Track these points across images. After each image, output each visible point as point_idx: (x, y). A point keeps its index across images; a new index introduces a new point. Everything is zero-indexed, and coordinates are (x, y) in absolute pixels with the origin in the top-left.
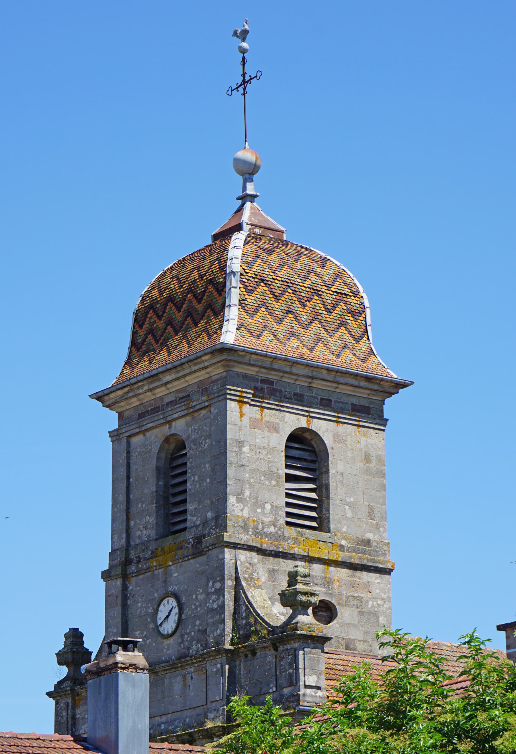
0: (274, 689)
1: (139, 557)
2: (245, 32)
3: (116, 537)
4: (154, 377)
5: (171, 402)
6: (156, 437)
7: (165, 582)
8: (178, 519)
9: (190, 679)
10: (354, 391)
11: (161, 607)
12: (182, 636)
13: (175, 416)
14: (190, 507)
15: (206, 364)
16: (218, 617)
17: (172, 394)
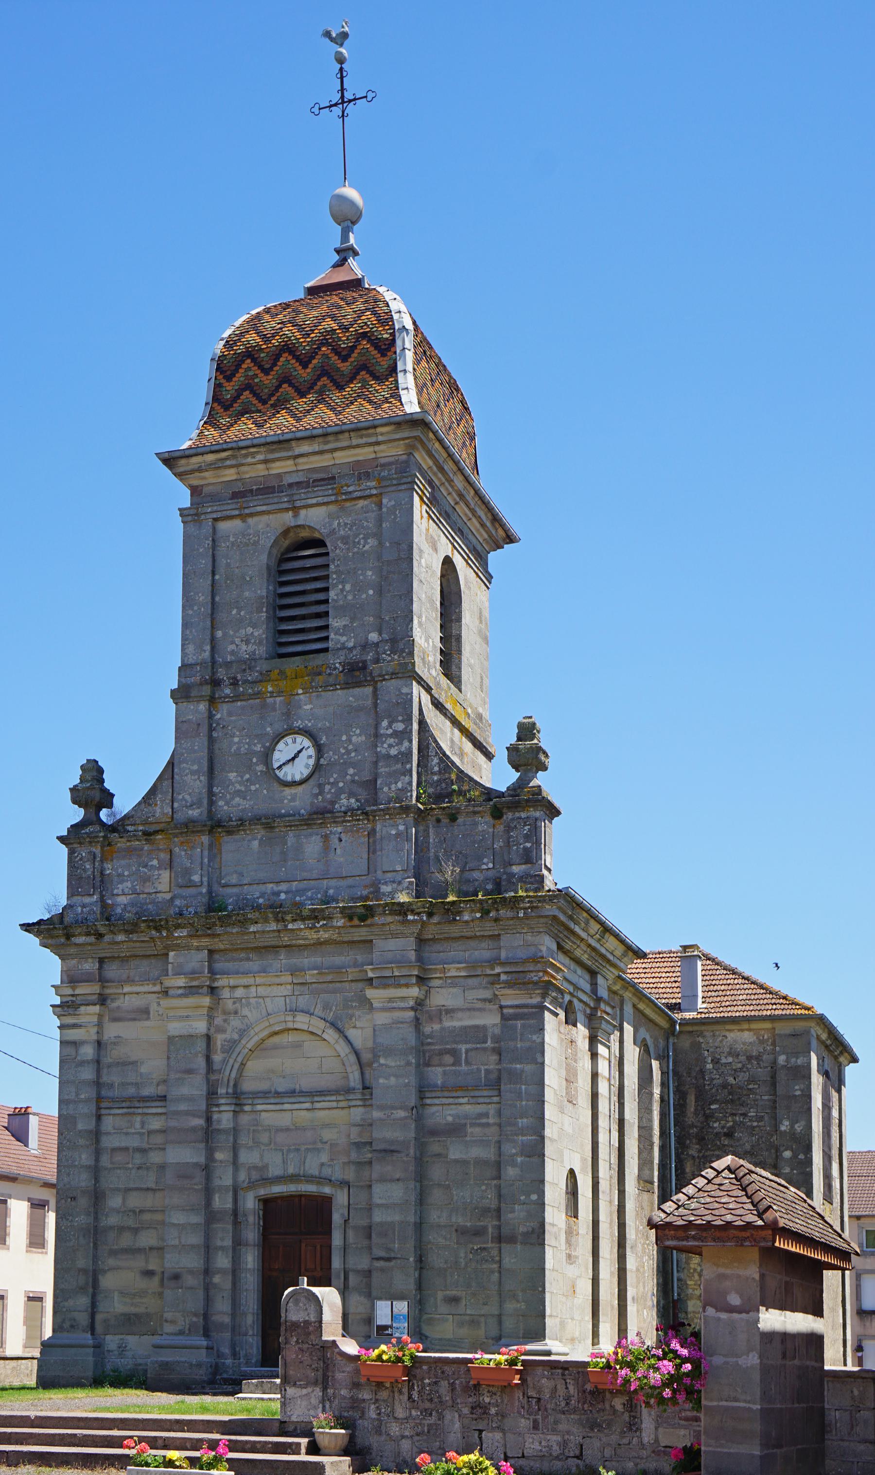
0: (491, 865)
1: (235, 678)
2: (345, 35)
3: (191, 648)
4: (282, 443)
5: (297, 483)
6: (268, 526)
7: (288, 714)
8: (291, 639)
9: (336, 841)
10: (478, 530)
11: (281, 745)
12: (320, 786)
13: (259, 509)
14: (335, 623)
15: (380, 438)
16: (399, 766)
17: (301, 473)
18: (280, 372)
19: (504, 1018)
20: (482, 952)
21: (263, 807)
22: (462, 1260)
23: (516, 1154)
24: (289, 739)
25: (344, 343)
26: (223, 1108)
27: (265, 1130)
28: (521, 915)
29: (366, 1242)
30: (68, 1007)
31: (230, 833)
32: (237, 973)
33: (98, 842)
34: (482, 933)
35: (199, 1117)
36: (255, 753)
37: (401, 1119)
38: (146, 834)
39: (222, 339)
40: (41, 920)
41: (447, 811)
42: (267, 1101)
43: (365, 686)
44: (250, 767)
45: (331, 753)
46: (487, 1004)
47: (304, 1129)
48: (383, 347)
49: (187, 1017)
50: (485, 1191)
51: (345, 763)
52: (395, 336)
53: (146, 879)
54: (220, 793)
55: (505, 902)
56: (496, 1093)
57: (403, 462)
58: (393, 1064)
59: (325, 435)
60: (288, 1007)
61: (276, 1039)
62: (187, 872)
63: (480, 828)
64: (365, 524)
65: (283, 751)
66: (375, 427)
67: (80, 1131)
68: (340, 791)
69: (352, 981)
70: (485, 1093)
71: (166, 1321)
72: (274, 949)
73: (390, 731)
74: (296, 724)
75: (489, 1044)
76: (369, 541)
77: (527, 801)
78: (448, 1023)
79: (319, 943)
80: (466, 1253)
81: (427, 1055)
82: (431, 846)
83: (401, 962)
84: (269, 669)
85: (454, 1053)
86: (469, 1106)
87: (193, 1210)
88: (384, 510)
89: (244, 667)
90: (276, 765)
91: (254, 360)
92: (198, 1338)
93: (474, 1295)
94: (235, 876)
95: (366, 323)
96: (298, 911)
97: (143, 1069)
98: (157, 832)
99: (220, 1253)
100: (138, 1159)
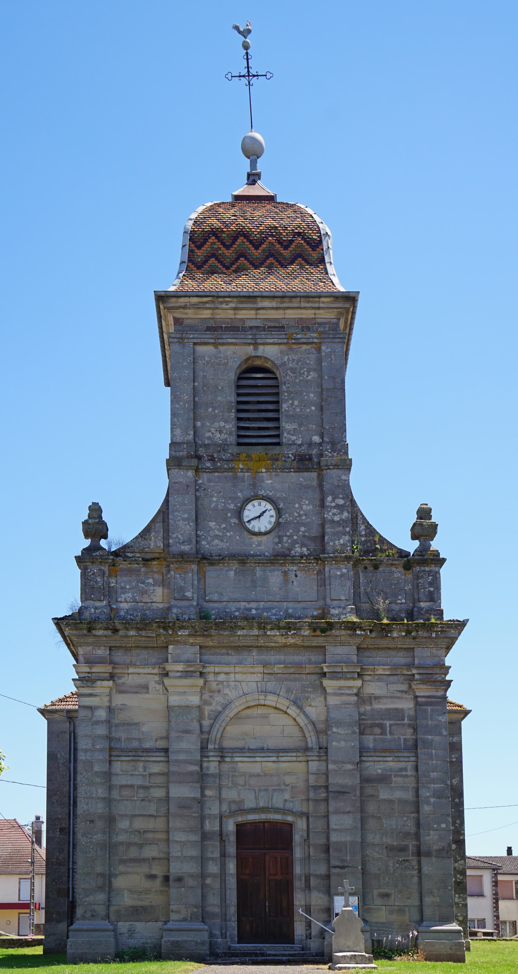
0: (404, 601)
2: (249, 31)
3: (178, 432)
4: (251, 298)
6: (234, 353)
11: (249, 506)
12: (280, 537)
13: (230, 341)
15: (322, 305)
17: (259, 321)
18: (238, 249)
19: (417, 704)
20: (401, 659)
21: (236, 548)
22: (391, 868)
23: (430, 797)
24: (256, 503)
25: (285, 237)
26: (211, 759)
27: (241, 776)
28: (434, 635)
29: (323, 855)
30: (87, 681)
31: (211, 564)
32: (220, 663)
33: (107, 563)
34: (402, 646)
35: (195, 765)
36: (230, 510)
37: (349, 770)
38: (145, 560)
39: (191, 219)
40: (66, 616)
41: (374, 562)
42: (243, 755)
43: (312, 472)
44: (225, 520)
45: (287, 515)
46: (404, 694)
47: (271, 775)
48: (313, 244)
49: (184, 692)
50: (406, 821)
51: (298, 523)
52: (321, 238)
53: (144, 592)
54: (203, 535)
55: (424, 626)
56: (413, 755)
57: (334, 324)
58: (343, 732)
59: (283, 297)
60: (259, 689)
61: (249, 712)
62: (182, 589)
63: (396, 575)
64: (308, 361)
65: (251, 510)
66: (320, 297)
67: (96, 772)
68: (295, 542)
69: (308, 674)
70: (406, 754)
71: (172, 911)
72: (248, 648)
73: (333, 504)
74: (260, 493)
75: (406, 721)
76: (311, 373)
77: (432, 560)
78: (376, 706)
79: (285, 646)
80: (394, 863)
81: (362, 727)
82: (361, 585)
83: (348, 663)
84: (239, 452)
85: (382, 727)
86: (393, 763)
87: (191, 831)
88: (323, 354)
89: (219, 449)
90: (246, 520)
91: (217, 237)
92: (199, 924)
93: (400, 892)
94: (216, 595)
95: (299, 226)
96: (277, 623)
97: (144, 729)
98: (153, 559)
99: (211, 862)
100: (142, 794)
